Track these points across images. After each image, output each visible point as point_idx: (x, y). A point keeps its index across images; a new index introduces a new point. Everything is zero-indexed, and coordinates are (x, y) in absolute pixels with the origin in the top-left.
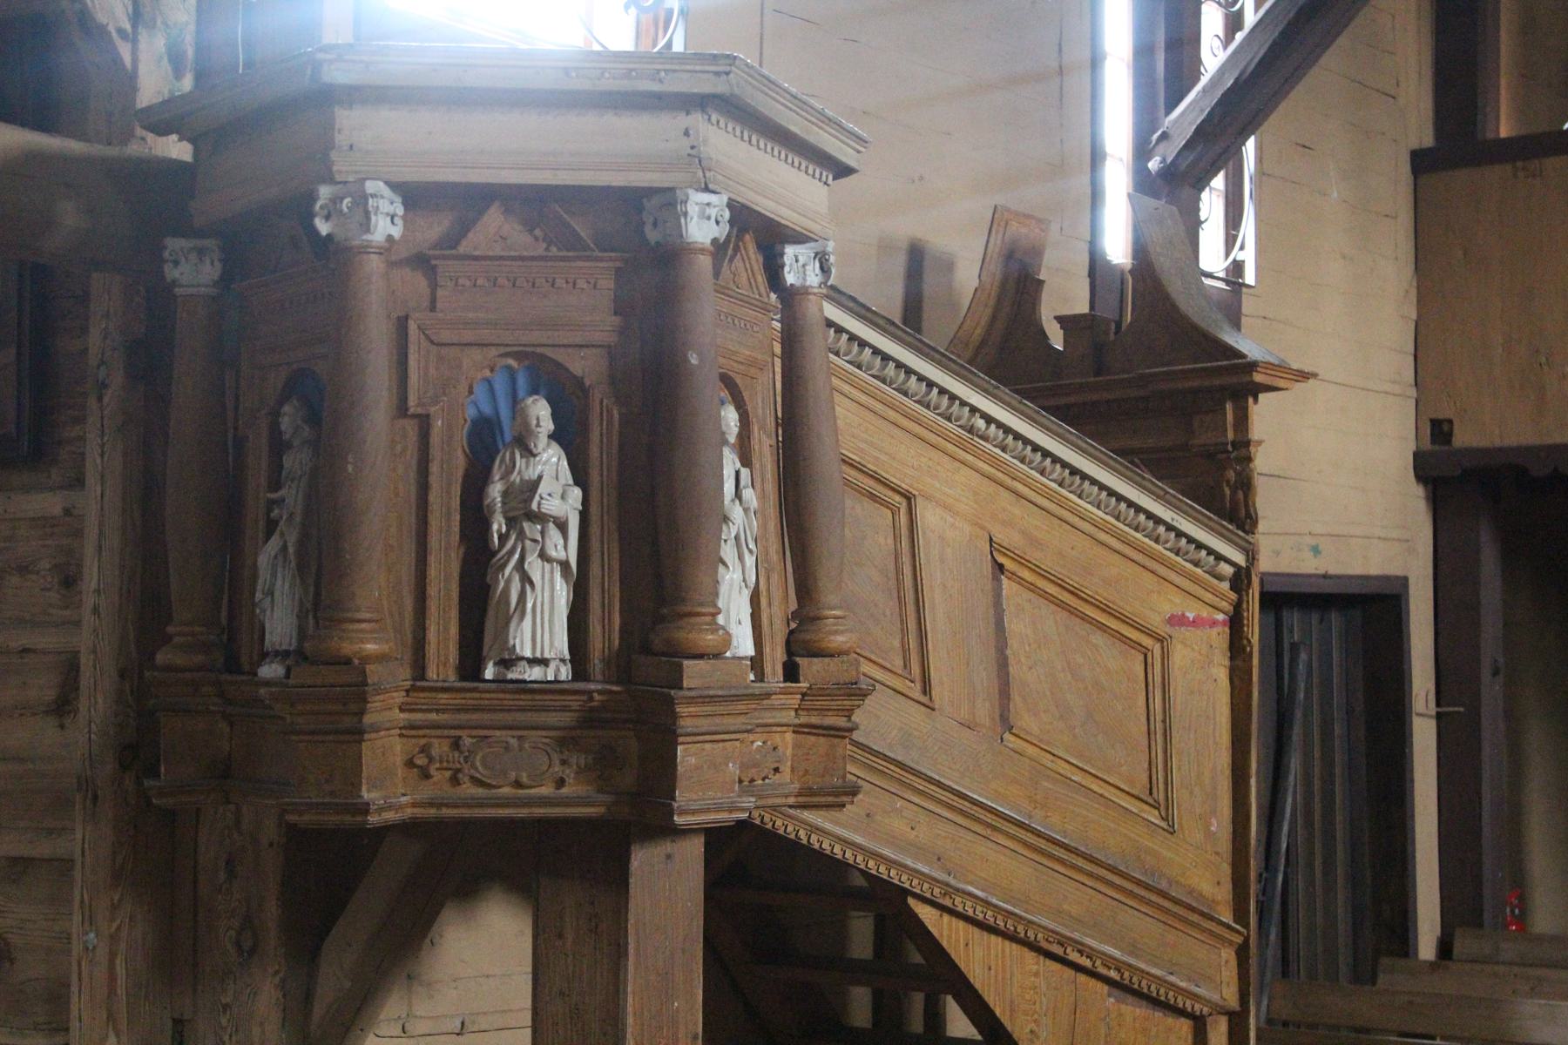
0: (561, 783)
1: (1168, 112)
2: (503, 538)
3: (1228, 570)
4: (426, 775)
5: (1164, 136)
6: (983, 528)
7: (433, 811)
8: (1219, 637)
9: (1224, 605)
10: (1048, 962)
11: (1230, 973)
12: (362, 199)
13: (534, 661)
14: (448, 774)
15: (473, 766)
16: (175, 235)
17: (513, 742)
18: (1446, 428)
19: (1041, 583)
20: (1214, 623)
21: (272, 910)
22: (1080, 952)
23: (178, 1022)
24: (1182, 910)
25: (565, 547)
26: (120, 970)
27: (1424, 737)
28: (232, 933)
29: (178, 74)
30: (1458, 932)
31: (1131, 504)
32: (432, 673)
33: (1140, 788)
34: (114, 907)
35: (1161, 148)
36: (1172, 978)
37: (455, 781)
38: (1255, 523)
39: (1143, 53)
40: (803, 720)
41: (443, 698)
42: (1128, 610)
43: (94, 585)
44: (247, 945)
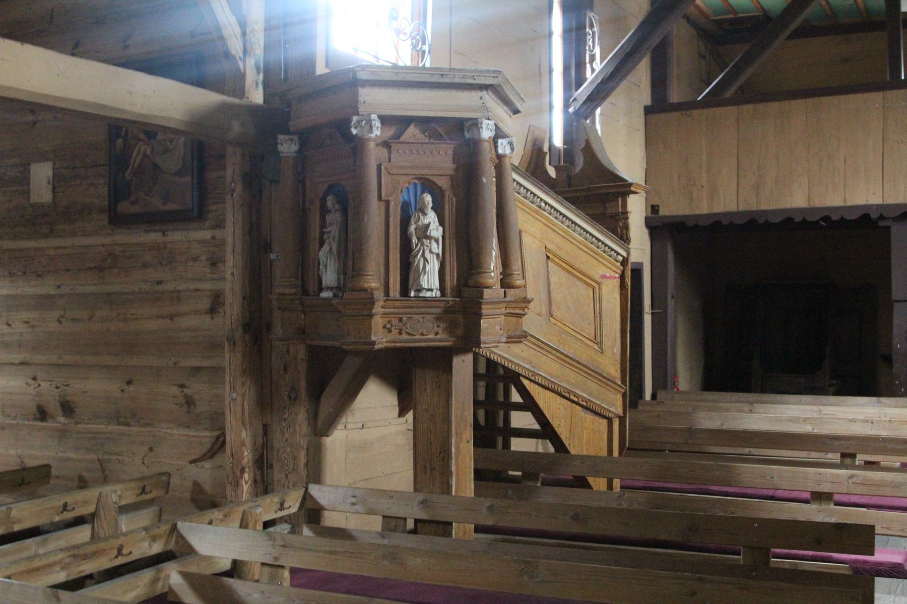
0: (437, 334)
1: (576, 90)
2: (417, 245)
3: (620, 258)
4: (390, 331)
5: (575, 99)
7: (393, 344)
8: (617, 282)
11: (620, 402)
12: (369, 122)
16: (282, 134)
17: (421, 320)
19: (561, 263)
21: (303, 383)
23: (265, 426)
25: (437, 248)
26: (246, 407)
29: (258, 73)
30: (659, 391)
31: (591, 234)
32: (391, 294)
33: (592, 338)
34: (243, 384)
37: (400, 333)
38: (630, 241)
39: (566, 69)
41: (397, 303)
42: (588, 273)
43: (231, 265)
44: (293, 396)
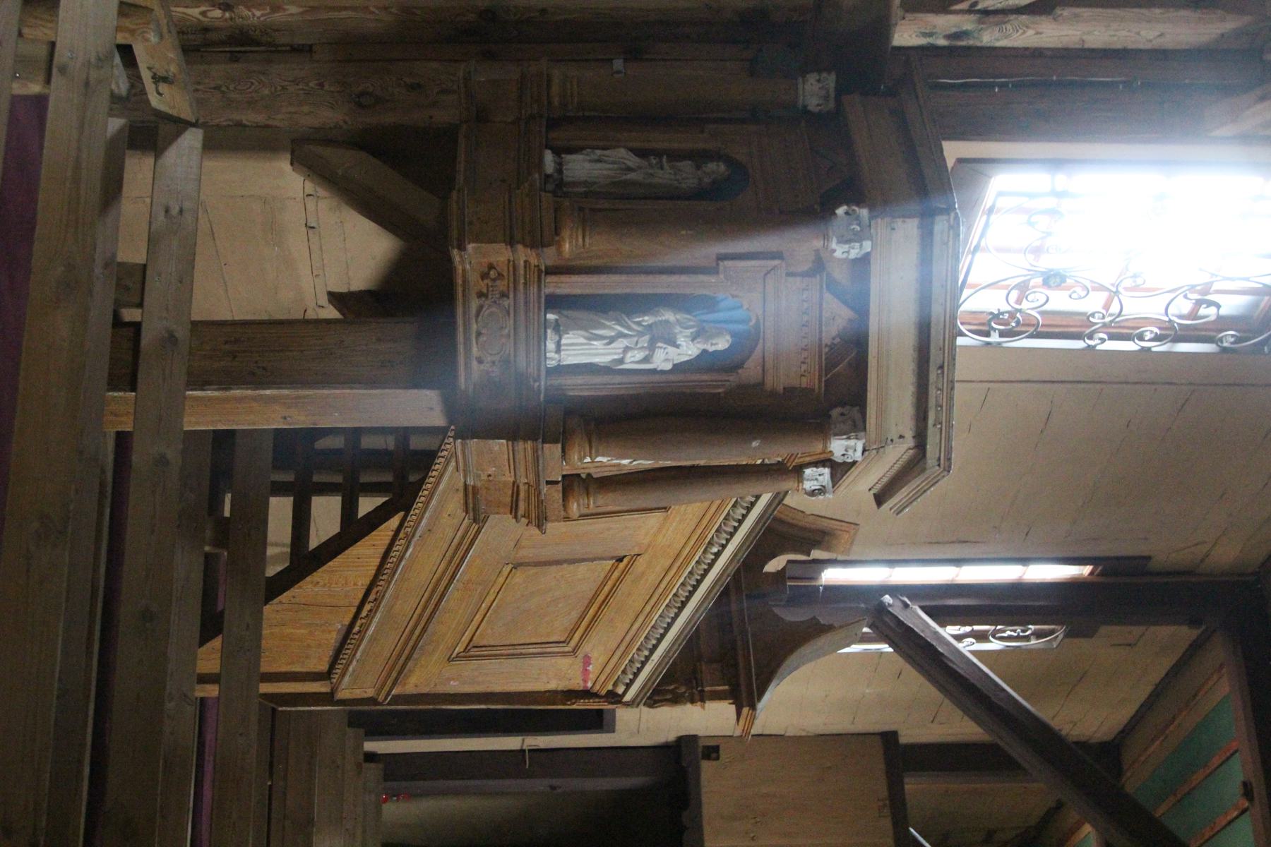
0: (480, 361)
1: (922, 608)
3: (620, 690)
4: (484, 276)
5: (906, 606)
6: (646, 550)
7: (460, 282)
8: (577, 683)
9: (597, 688)
10: (363, 591)
11: (358, 693)
12: (858, 238)
13: (558, 345)
14: (485, 291)
15: (490, 306)
18: (714, 755)
19: (610, 583)
20: (585, 681)
21: (389, 119)
22: (370, 611)
24: (401, 663)
26: (344, 14)
27: (511, 743)
28: (371, 89)
31: (663, 636)
35: (899, 604)
36: (354, 662)
38: (651, 706)
40: (522, 488)
42: (593, 633)
